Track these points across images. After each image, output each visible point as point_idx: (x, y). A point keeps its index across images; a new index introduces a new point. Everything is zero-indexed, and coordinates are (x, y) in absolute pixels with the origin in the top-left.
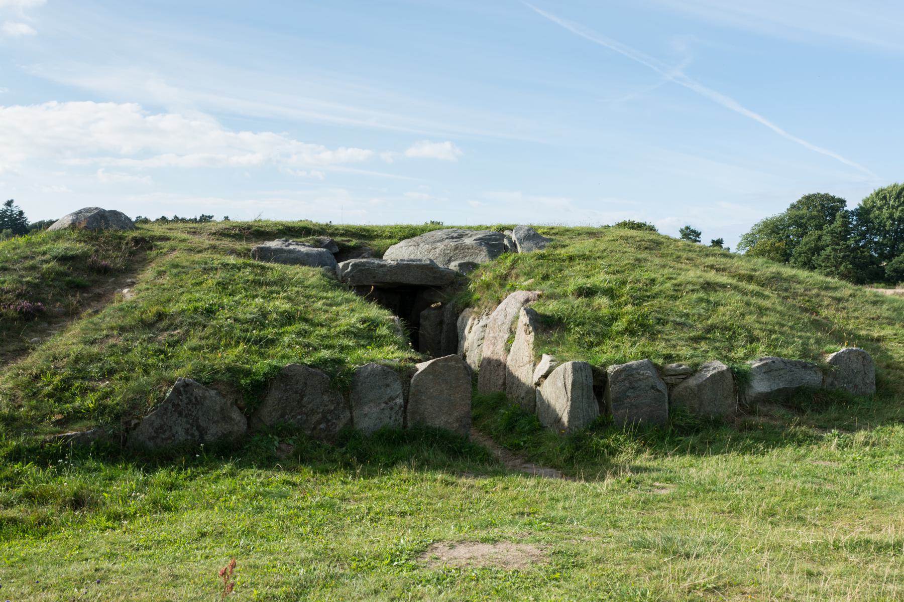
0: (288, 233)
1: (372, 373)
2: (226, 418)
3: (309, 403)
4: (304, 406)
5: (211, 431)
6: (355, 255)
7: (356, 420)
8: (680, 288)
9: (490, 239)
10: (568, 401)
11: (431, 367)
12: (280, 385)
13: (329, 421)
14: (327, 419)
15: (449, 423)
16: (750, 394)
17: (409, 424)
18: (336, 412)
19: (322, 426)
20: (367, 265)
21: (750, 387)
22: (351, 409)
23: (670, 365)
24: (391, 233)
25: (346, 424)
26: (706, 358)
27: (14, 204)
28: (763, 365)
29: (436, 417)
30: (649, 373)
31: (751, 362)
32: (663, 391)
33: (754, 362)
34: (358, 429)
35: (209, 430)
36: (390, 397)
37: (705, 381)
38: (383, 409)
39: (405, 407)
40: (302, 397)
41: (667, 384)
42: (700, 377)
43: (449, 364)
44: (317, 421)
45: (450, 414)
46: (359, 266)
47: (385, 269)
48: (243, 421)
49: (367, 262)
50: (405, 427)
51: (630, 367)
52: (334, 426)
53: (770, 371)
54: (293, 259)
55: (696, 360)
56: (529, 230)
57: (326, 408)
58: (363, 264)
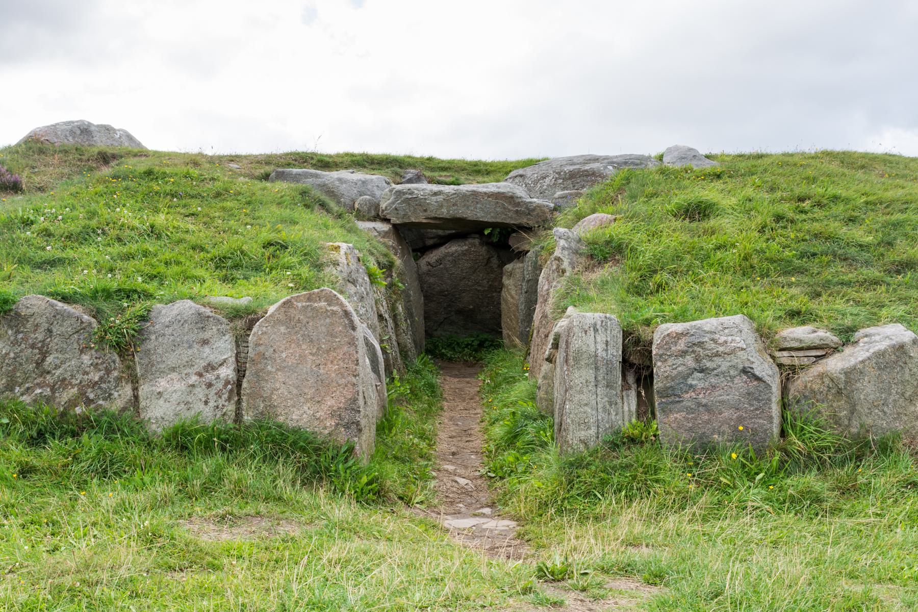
3: (57, 367)
7: (143, 404)
17: (247, 418)
22: (135, 381)
39: (239, 384)
40: (44, 355)
41: (780, 366)
47: (440, 198)
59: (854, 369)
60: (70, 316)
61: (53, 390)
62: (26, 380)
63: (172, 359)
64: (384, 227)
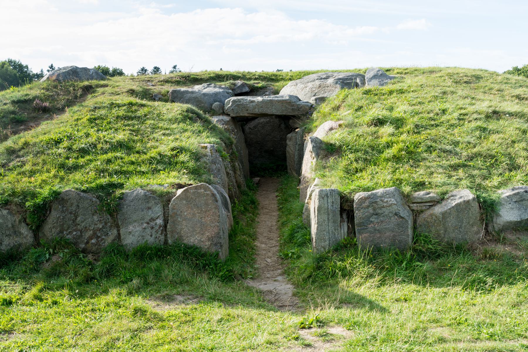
0: (217, 79)
1: (137, 197)
2: (17, 233)
3: (82, 222)
4: (79, 225)
5: (5, 243)
6: (261, 93)
7: (122, 237)
8: (464, 117)
9: (347, 79)
10: (315, 224)
11: (184, 193)
12: (58, 207)
13: (99, 237)
14: (97, 235)
15: (203, 242)
16: (498, 222)
17: (170, 241)
18: (104, 230)
19: (93, 241)
20: (242, 101)
21: (498, 215)
22: (118, 227)
23: (417, 193)
24: (292, 76)
25: (114, 240)
26: (457, 186)
27: (177, 67)
28: (515, 194)
29: (191, 236)
30: (393, 201)
31: (503, 191)
32: (406, 217)
33: (505, 191)
34: (124, 244)
35: (3, 242)
36: (151, 218)
37: (450, 209)
38: (145, 228)
39: (165, 226)
41: (413, 210)
42: (445, 205)
43: (199, 191)
44: (89, 237)
45: (202, 234)
46: (236, 102)
47: (254, 104)
48: (29, 235)
49: (242, 99)
50: (166, 242)
51: (375, 195)
52: (103, 241)
53: (522, 201)
54: (194, 97)
55: (448, 188)
56: (379, 71)
57: (96, 226)
58: (239, 101)
59: (446, 212)
60: (87, 199)
61: (81, 232)
62: (68, 228)
63: (134, 217)
64: (226, 118)
